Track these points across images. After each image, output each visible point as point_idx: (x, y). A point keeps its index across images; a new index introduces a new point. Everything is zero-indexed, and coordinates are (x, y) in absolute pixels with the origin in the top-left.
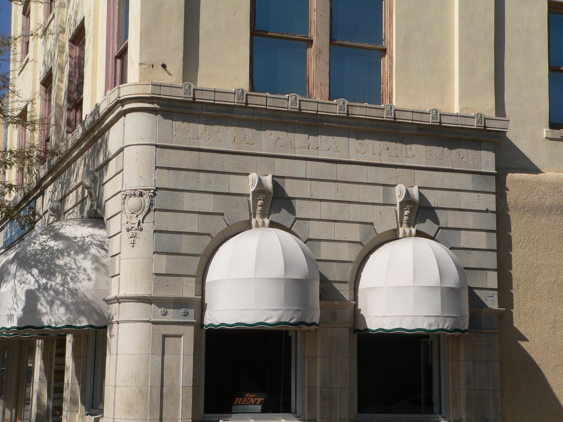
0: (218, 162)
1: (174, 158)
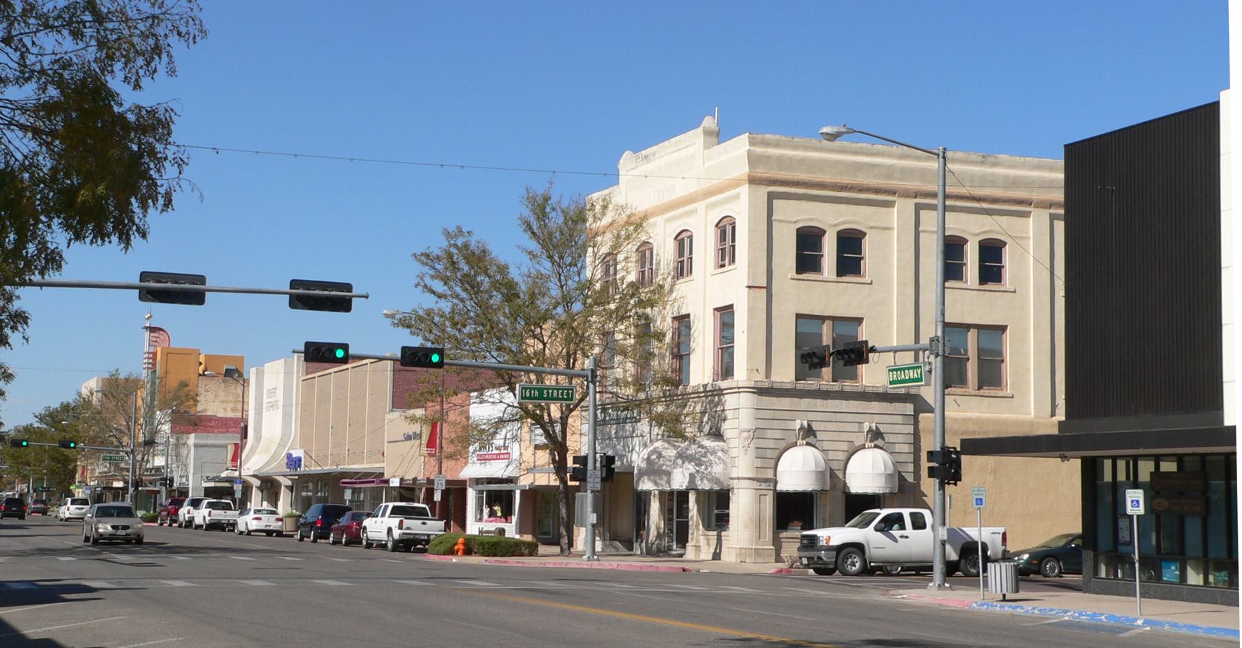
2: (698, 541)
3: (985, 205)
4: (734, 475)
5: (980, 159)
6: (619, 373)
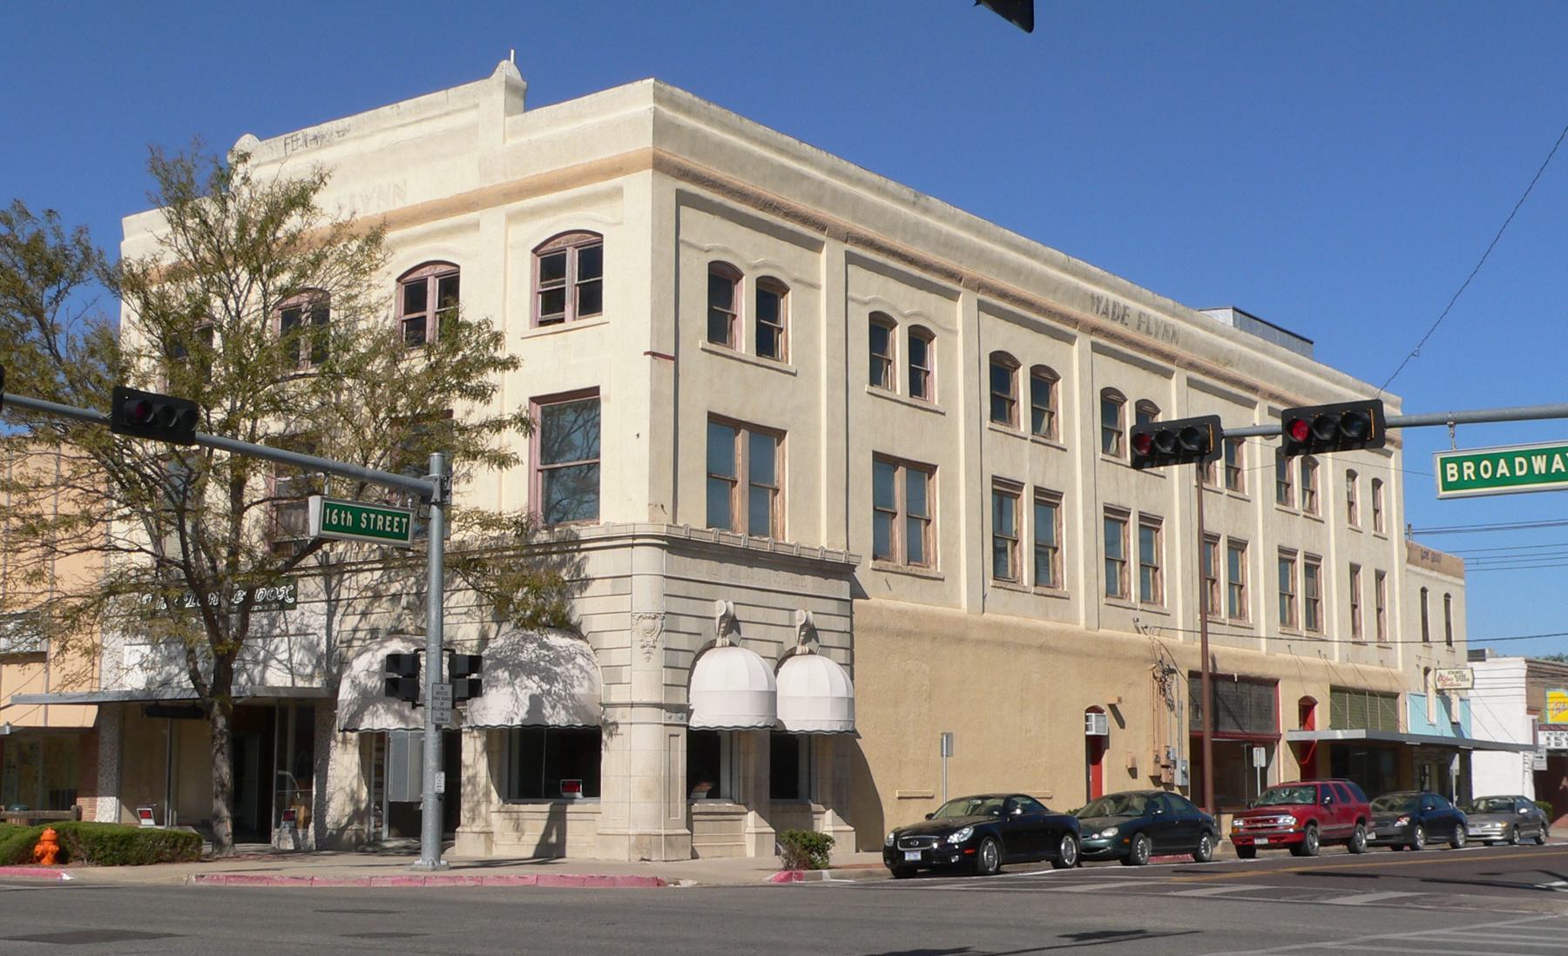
0: (695, 590)
1: (678, 588)
2: (488, 823)
3: (916, 272)
4: (614, 700)
5: (912, 198)
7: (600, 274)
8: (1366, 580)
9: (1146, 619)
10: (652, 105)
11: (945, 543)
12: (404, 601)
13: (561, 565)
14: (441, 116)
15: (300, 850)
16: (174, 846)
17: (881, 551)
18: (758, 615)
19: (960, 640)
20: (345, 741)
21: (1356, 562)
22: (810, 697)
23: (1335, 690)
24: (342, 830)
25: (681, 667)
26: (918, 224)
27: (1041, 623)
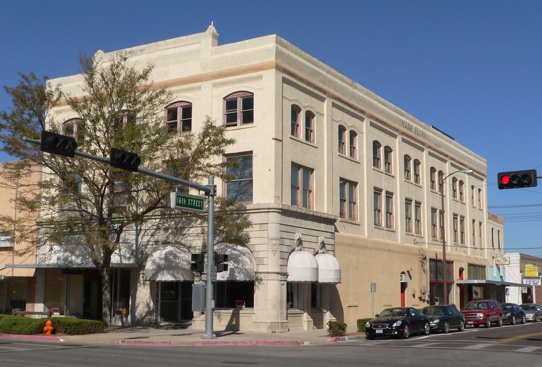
1: (284, 228)
3: (352, 110)
4: (260, 271)
6: (91, 175)
7: (253, 108)
8: (477, 223)
9: (418, 240)
10: (275, 44)
11: (361, 211)
12: (170, 231)
13: (238, 218)
14: (184, 45)
15: (123, 327)
16: (95, 327)
17: (342, 214)
18: (308, 238)
19: (366, 247)
20: (144, 284)
21: (474, 219)
22: (327, 268)
23: (470, 265)
24: (143, 318)
25: (285, 258)
26: (353, 92)
27: (388, 241)
